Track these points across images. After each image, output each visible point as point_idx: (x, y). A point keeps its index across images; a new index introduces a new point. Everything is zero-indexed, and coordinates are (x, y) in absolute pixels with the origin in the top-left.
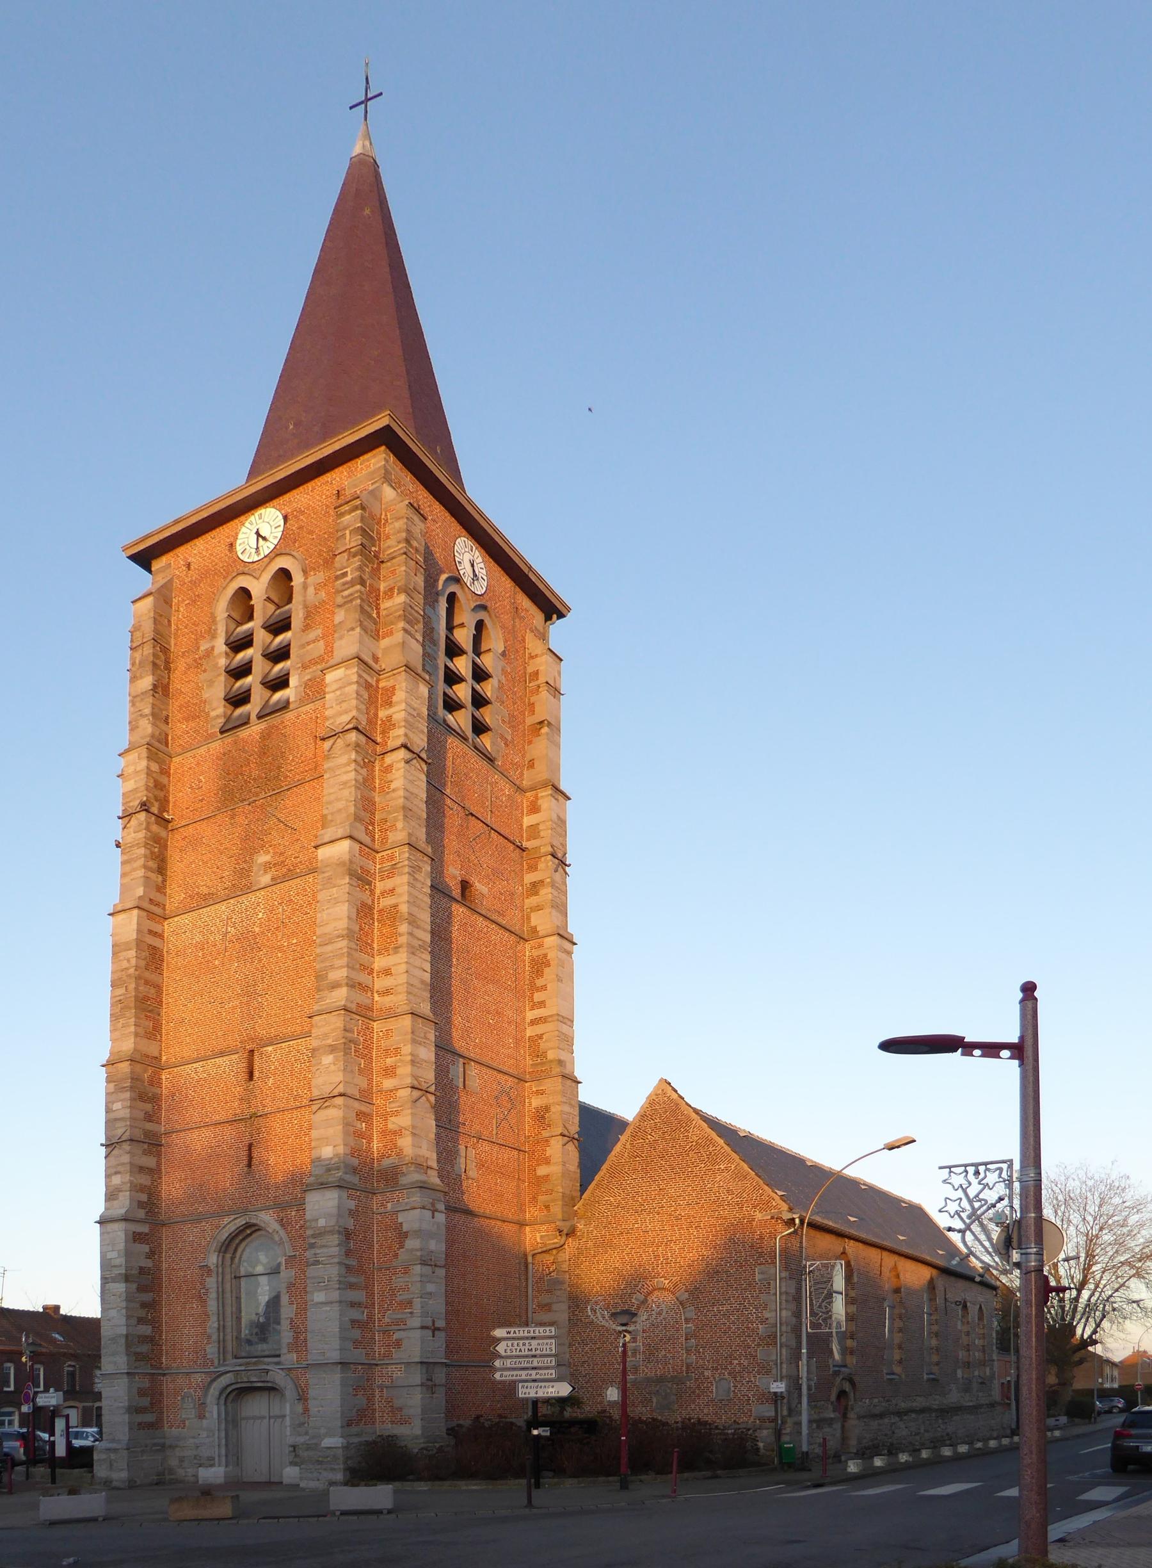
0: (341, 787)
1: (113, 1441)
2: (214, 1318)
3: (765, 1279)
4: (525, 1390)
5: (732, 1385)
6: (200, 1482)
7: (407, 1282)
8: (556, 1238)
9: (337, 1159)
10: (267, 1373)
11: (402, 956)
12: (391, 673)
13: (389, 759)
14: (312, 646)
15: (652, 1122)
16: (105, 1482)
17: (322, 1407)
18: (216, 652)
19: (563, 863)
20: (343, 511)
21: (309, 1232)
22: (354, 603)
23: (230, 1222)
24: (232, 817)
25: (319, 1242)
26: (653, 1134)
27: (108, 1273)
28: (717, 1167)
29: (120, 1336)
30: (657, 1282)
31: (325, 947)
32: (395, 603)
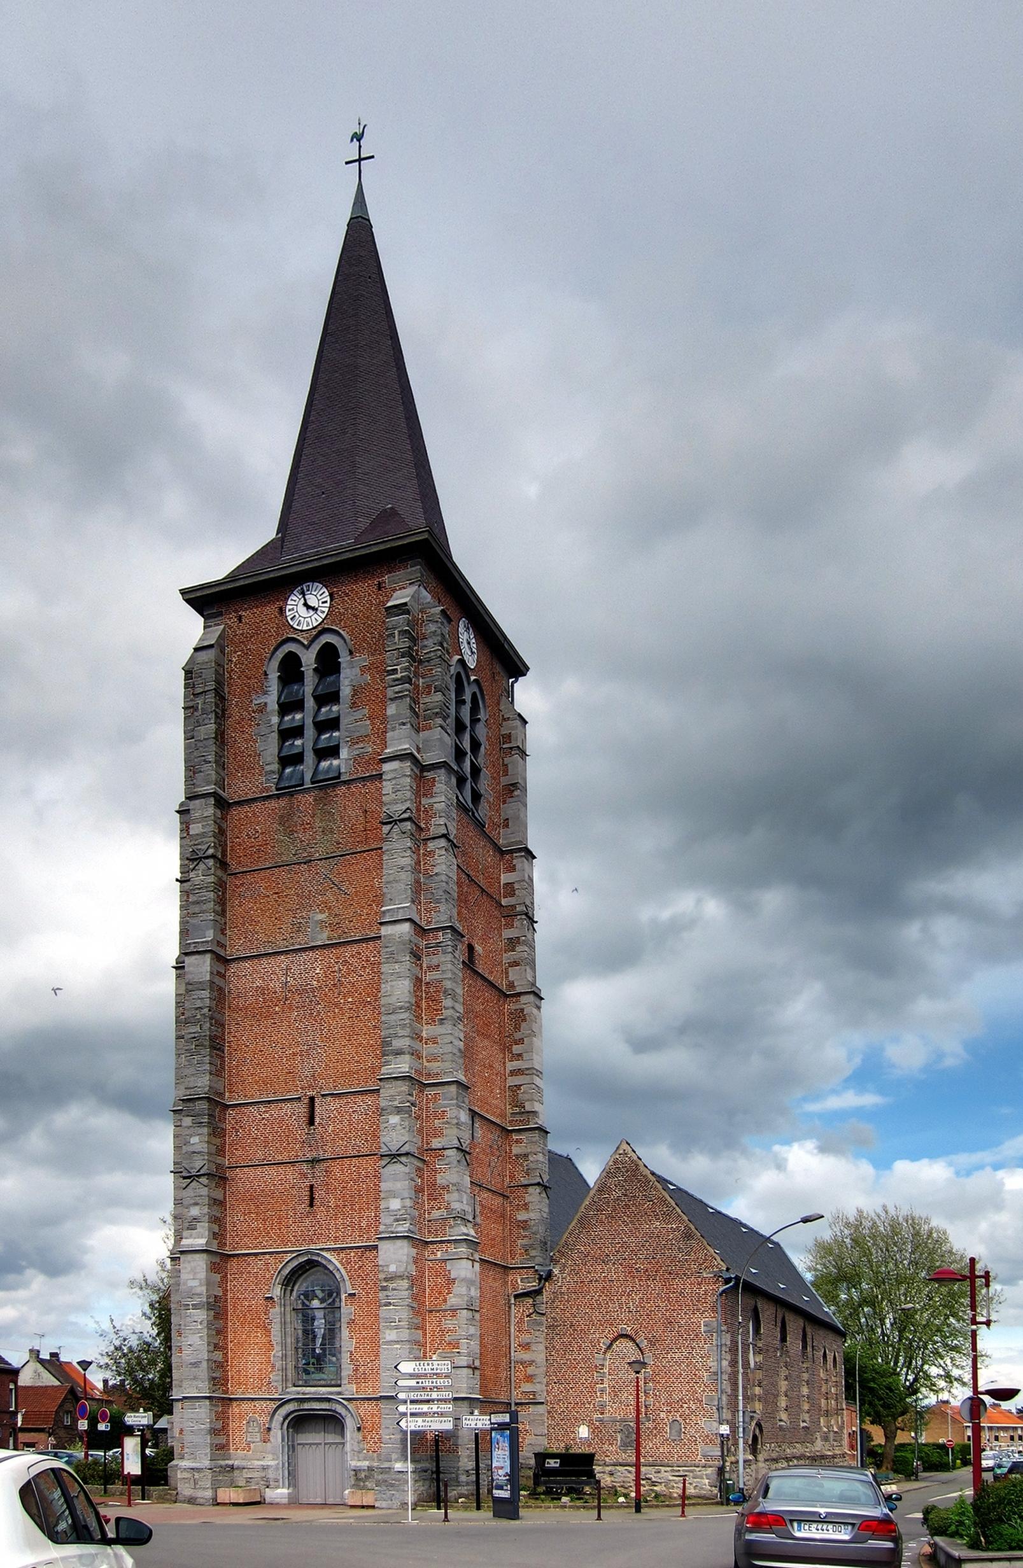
2: (277, 1348)
3: (709, 1331)
4: (468, 1422)
5: (683, 1426)
8: (535, 1281)
11: (447, 1028)
13: (431, 845)
15: (616, 1179)
17: (393, 1434)
18: (269, 708)
19: (533, 921)
21: (382, 1276)
26: (617, 1191)
27: (189, 1300)
28: (670, 1226)
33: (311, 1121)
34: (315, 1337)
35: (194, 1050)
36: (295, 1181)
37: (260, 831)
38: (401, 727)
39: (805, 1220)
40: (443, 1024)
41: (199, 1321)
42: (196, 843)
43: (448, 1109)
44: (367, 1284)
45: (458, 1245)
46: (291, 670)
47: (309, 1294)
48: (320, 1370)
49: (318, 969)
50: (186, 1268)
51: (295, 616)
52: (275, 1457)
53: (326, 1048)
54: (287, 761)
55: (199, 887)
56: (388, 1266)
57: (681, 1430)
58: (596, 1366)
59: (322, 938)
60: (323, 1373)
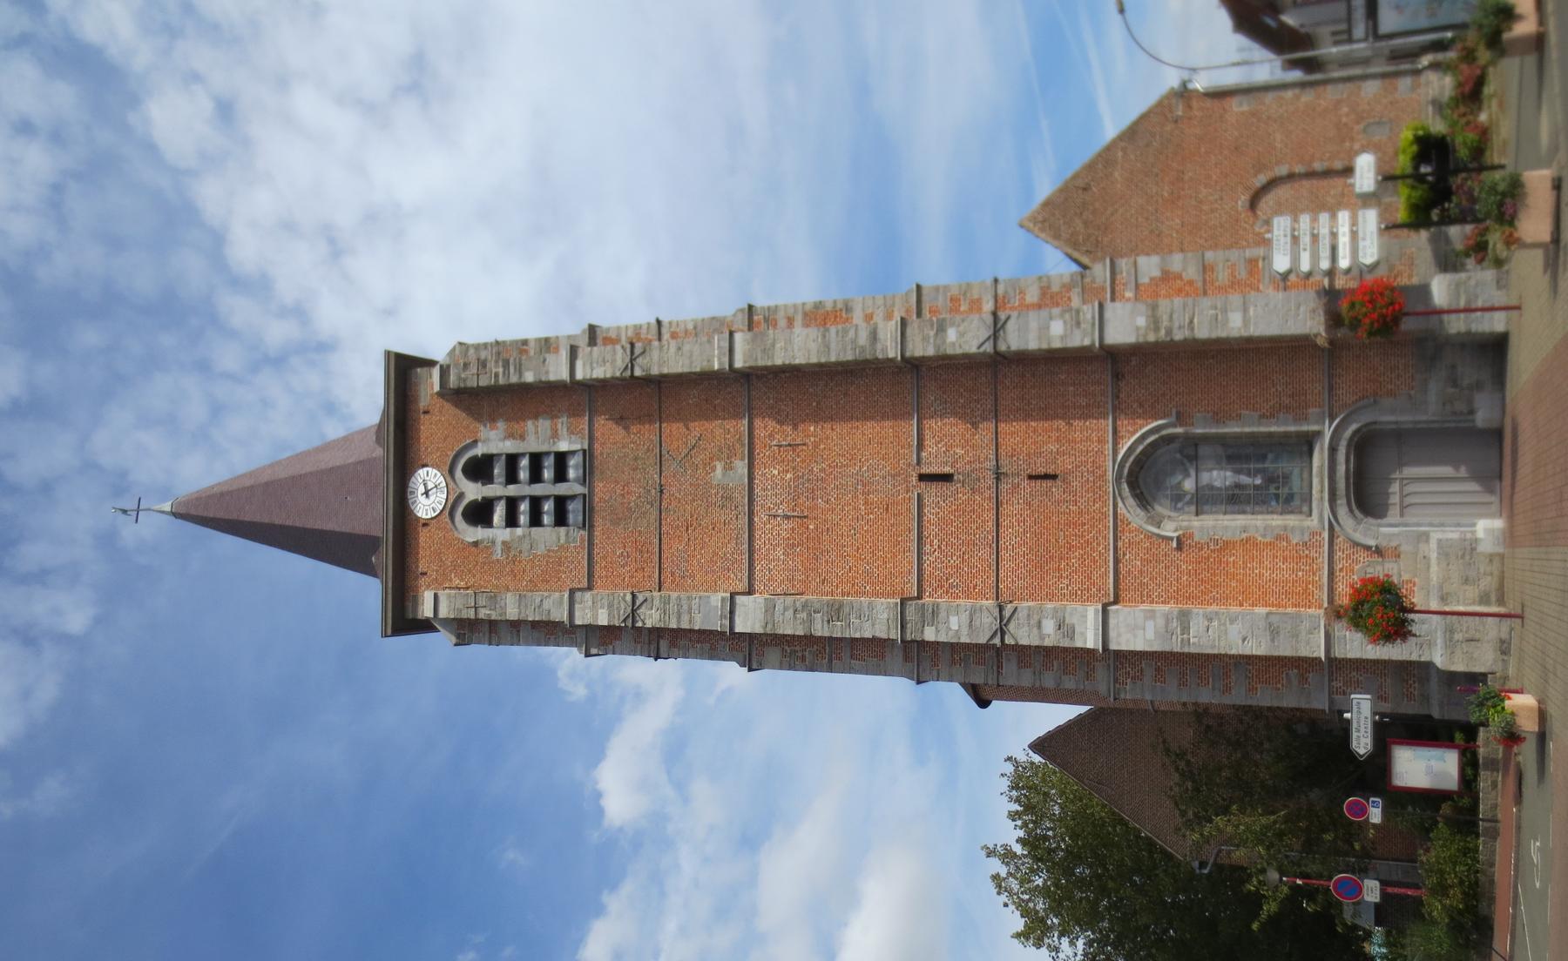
6: (1500, 550)
7: (1224, 266)
33: (947, 478)
34: (1238, 486)
35: (843, 623)
37: (622, 550)
39: (1122, 11)
41: (1206, 623)
42: (616, 616)
45: (1118, 270)
46: (479, 513)
47: (1176, 494)
50: (1128, 641)
51: (433, 508)
53: (863, 460)
56: (1138, 329)
59: (741, 467)
60: (1291, 473)
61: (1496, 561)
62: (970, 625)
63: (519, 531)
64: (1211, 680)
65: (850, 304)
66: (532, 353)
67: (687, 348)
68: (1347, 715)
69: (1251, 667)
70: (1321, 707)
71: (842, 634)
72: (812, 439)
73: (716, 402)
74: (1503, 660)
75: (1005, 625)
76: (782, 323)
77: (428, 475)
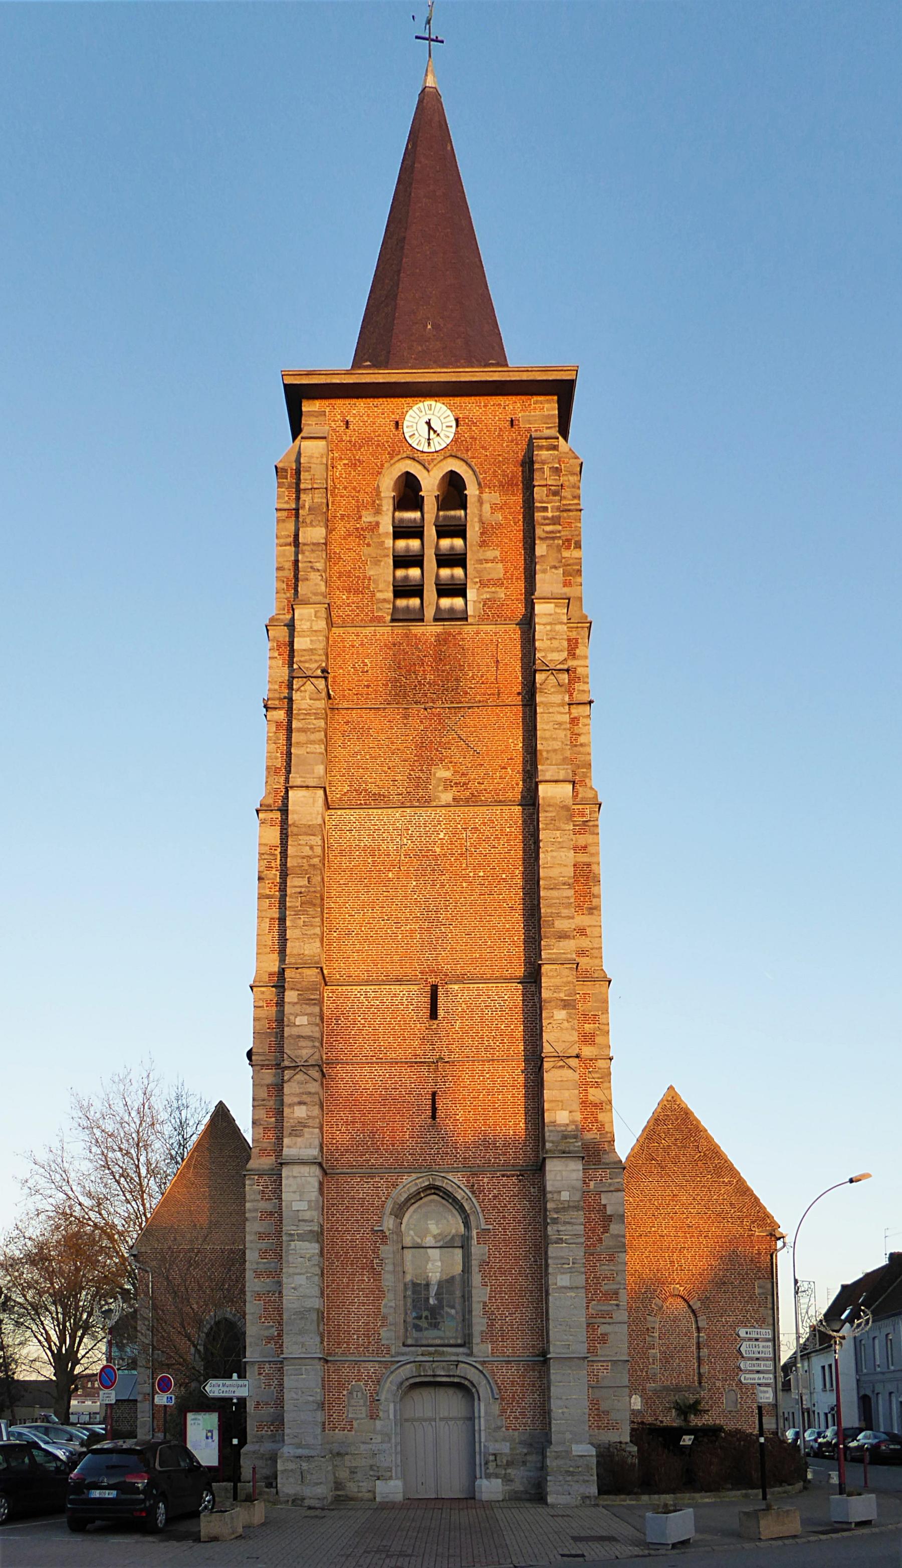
0: (556, 726)
1: (299, 1446)
3: (763, 1293)
7: (613, 1270)
9: (574, 1127)
10: (457, 1365)
12: (576, 625)
14: (490, 565)
15: (665, 1127)
16: (294, 1501)
18: (382, 529)
20: (540, 444)
22: (556, 541)
23: (412, 1181)
24: (406, 717)
25: (563, 1217)
26: (666, 1139)
27: (294, 1228)
29: (309, 1310)
30: (674, 1289)
31: (551, 891)
32: (573, 556)
33: (434, 1015)
35: (299, 908)
36: (413, 1086)
38: (553, 570)
40: (592, 914)
41: (308, 1256)
43: (600, 1013)
44: (504, 1217)
48: (436, 1326)
49: (441, 833)
52: (387, 1439)
54: (402, 590)
55: (305, 712)
57: (737, 1400)
58: (648, 1329)
60: (438, 1329)
61: (369, 1496)
62: (299, 1037)
63: (389, 542)
64: (265, 1260)
65: (595, 912)
66: (566, 554)
67: (561, 734)
68: (235, 1375)
69: (277, 1295)
70: (247, 1354)
71: (289, 907)
72: (471, 874)
73: (509, 769)
74: (288, 1501)
75: (301, 1070)
76: (582, 840)
77: (447, 426)
